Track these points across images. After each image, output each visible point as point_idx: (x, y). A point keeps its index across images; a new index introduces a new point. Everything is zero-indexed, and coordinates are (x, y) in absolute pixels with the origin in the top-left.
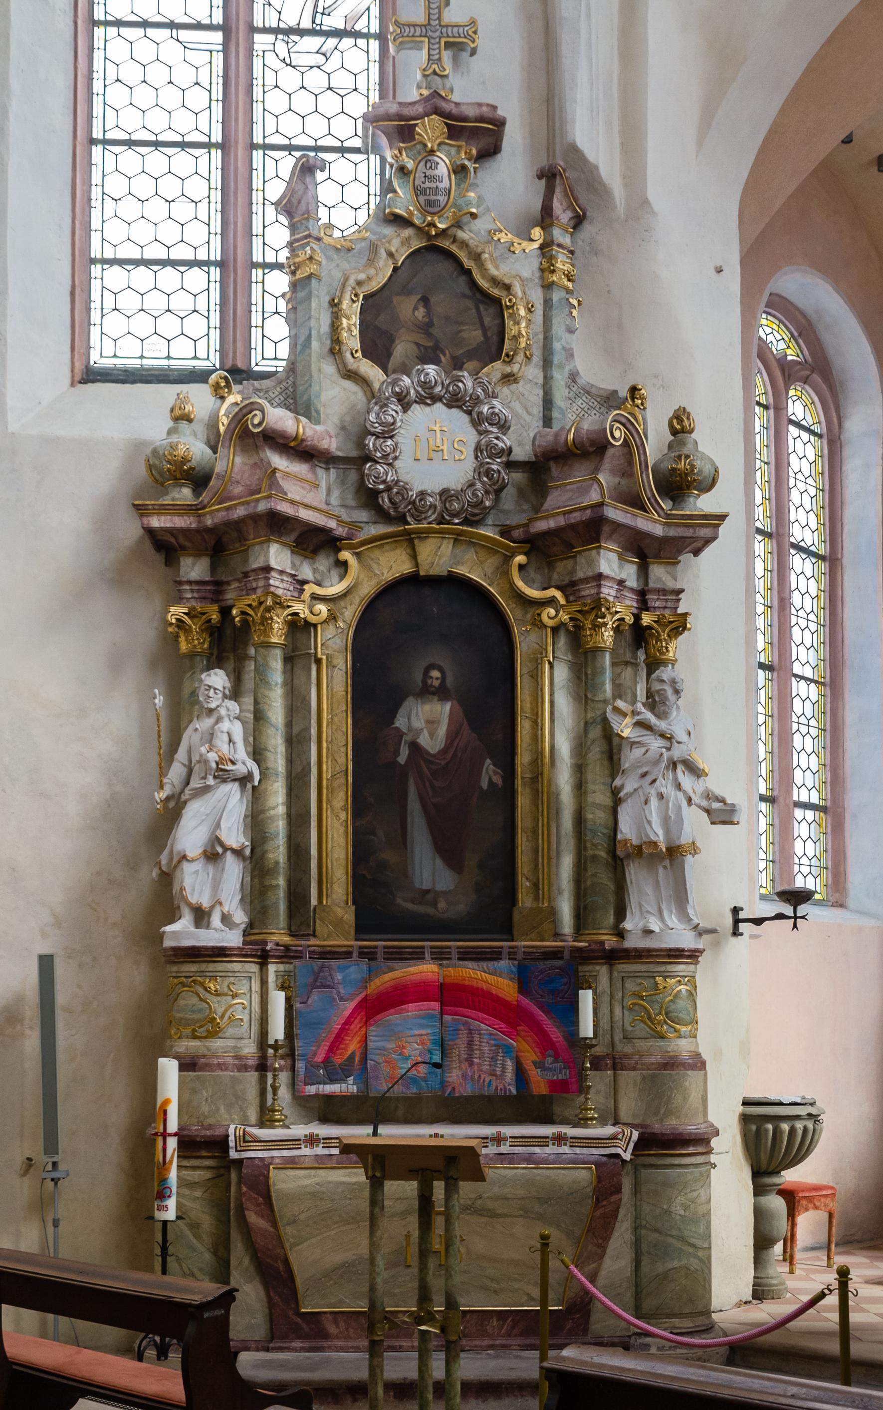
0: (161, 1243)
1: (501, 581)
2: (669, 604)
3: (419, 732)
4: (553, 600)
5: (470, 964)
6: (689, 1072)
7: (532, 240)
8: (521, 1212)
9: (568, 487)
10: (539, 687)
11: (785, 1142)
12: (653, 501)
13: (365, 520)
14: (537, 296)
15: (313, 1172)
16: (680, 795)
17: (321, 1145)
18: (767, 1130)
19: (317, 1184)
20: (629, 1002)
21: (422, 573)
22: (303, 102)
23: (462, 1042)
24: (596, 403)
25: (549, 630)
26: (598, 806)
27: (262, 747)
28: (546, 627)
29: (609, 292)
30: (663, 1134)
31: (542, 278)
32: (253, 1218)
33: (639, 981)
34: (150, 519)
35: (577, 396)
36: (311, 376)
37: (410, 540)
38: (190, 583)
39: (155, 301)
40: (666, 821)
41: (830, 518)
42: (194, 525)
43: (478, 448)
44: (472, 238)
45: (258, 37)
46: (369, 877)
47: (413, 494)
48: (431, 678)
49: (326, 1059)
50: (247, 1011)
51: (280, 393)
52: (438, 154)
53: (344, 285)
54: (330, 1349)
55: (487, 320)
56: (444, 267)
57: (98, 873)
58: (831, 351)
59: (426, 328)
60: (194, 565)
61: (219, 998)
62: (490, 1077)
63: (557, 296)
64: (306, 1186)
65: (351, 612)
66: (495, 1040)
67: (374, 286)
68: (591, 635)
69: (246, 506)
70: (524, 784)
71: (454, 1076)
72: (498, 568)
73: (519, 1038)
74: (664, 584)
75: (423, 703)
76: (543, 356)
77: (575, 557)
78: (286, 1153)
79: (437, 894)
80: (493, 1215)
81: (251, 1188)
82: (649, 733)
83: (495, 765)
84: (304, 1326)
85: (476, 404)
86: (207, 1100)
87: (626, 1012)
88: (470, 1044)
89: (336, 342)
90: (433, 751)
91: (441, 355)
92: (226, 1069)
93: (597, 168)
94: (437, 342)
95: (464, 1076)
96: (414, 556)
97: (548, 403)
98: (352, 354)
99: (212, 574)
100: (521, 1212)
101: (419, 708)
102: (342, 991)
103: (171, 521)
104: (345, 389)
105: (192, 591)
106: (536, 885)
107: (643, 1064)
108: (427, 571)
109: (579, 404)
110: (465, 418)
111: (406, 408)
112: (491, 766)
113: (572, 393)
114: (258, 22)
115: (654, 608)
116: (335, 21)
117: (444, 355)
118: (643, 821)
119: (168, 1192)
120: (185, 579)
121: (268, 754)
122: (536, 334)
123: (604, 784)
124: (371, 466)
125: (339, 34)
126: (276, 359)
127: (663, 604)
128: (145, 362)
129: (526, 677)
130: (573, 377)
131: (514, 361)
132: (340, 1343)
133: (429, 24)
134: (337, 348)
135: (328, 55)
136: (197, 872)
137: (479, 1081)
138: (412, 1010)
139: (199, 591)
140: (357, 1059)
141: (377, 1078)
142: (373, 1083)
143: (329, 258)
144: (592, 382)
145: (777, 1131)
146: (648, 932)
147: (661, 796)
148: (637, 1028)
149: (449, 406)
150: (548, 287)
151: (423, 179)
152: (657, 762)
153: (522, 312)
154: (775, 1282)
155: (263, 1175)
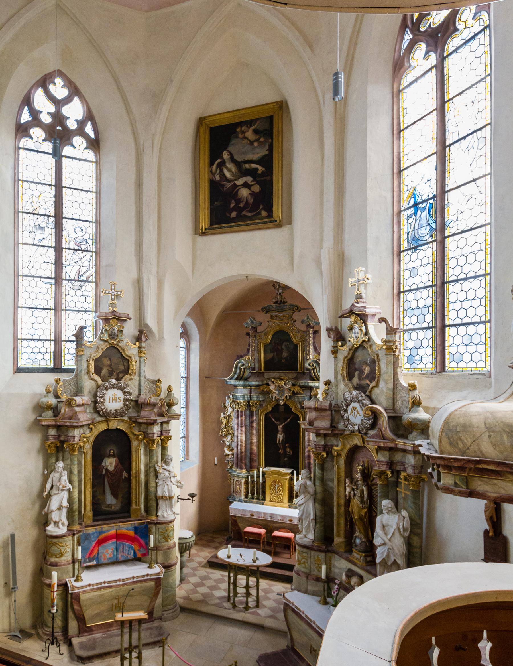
14: (137, 359)
22: (76, 299)
37: (107, 422)
40: (169, 490)
45: (64, 281)
49: (89, 557)
53: (90, 357)
55: (125, 364)
58: (188, 329)
59: (110, 366)
63: (142, 359)
65: (92, 440)
79: (112, 505)
88: (123, 548)
89: (88, 372)
96: (108, 425)
97: (140, 385)
110: (121, 392)
111: (107, 390)
118: (163, 491)
125: (85, 281)
128: (33, 366)
130: (145, 377)
132: (96, 632)
138: (110, 542)
145: (186, 545)
146: (164, 517)
150: (140, 357)
153: (134, 364)
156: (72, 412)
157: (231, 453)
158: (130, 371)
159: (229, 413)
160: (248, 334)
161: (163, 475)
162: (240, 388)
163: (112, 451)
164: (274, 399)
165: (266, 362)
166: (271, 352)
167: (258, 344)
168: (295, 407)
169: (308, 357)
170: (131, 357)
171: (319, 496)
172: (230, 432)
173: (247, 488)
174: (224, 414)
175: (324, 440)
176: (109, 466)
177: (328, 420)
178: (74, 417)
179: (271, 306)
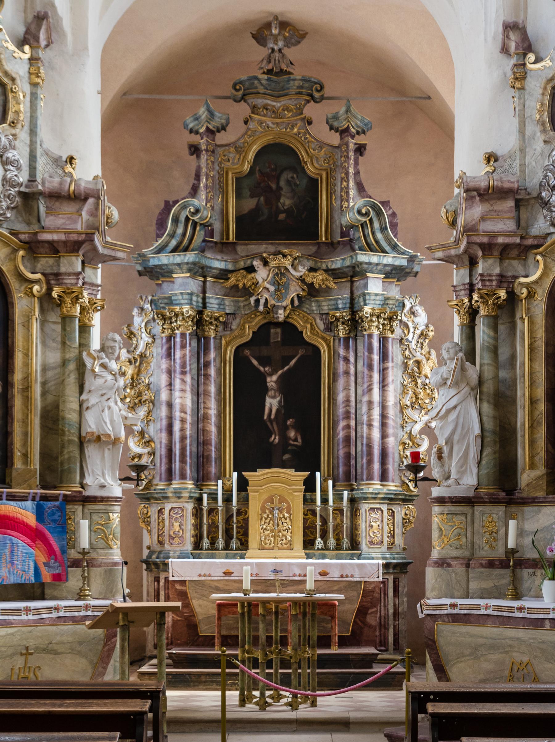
2: (94, 292)
4: (39, 281)
5: (12, 503)
7: (24, 53)
8: (70, 651)
10: (30, 333)
25: (36, 299)
28: (34, 296)
29: (58, 95)
68: (71, 307)
70: (18, 392)
72: (7, 256)
73: (36, 549)
76: (30, 126)
77: (59, 257)
82: (104, 370)
85: (5, 151)
87: (93, 533)
88: (12, 552)
93: (62, 19)
100: (70, 651)
118: (100, 421)
129: (21, 326)
144: (50, 149)
147: (109, 408)
148: (99, 542)
150: (35, 85)
152: (111, 388)
153: (21, 97)
157: (147, 450)
158: (10, 117)
159: (141, 348)
160: (195, 150)
161: (99, 381)
162: (180, 277)
164: (261, 308)
165: (239, 219)
166: (252, 196)
167: (221, 176)
168: (312, 328)
169: (345, 204)
170: (13, 80)
171: (489, 387)
172: (145, 397)
173: (198, 527)
174: (128, 352)
175: (500, 266)
177: (509, 218)
179: (256, 78)
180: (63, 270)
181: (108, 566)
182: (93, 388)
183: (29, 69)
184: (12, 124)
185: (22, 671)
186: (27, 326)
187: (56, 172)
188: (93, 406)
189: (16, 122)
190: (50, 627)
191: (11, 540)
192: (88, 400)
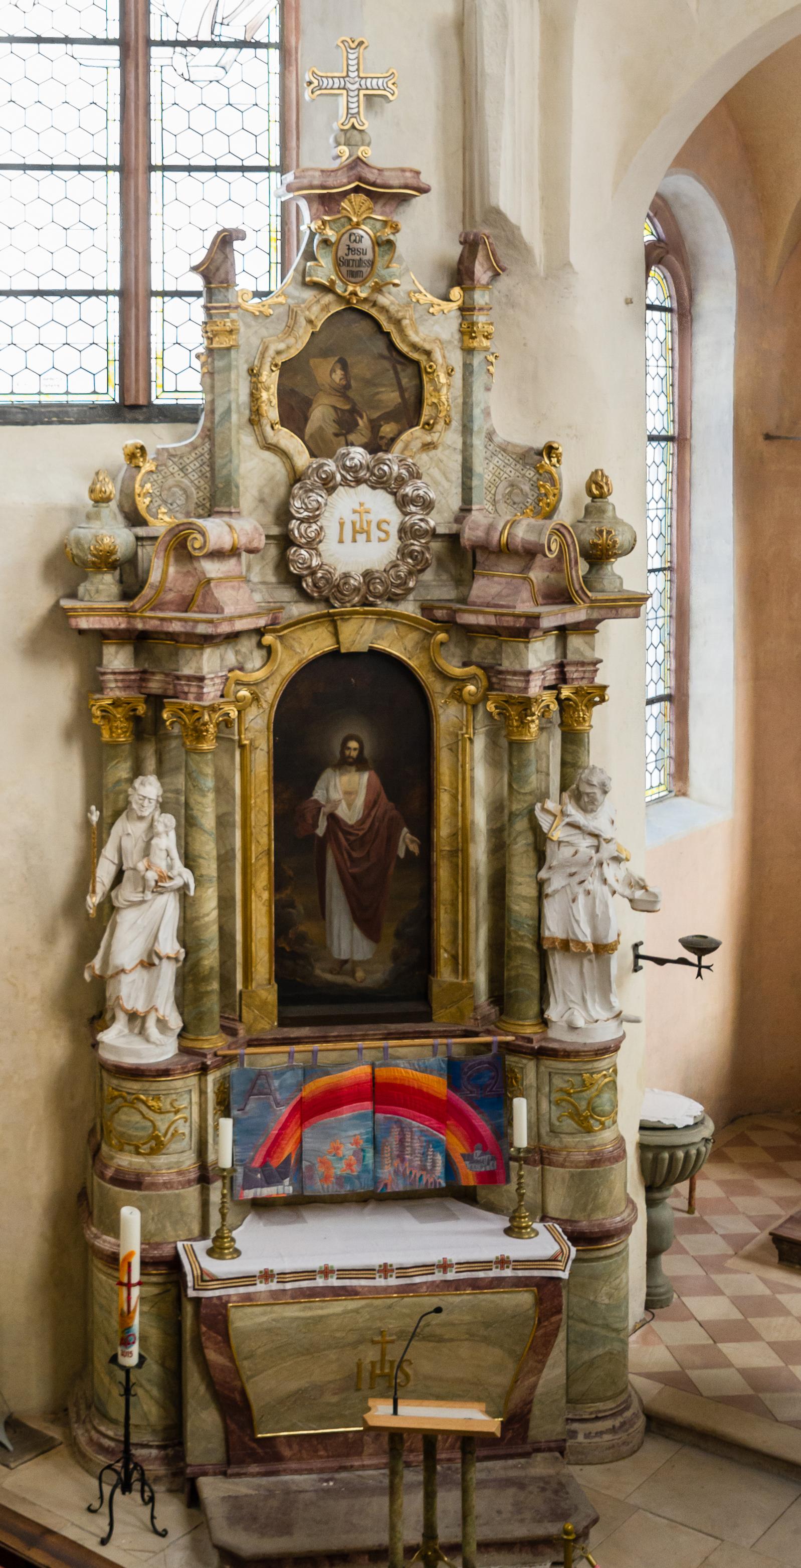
0: (124, 1383)
1: (421, 656)
3: (337, 804)
4: (474, 678)
6: (614, 1166)
8: (467, 1336)
9: (496, 579)
11: (680, 1168)
12: (580, 592)
13: (287, 600)
14: (456, 358)
15: (269, 1308)
16: (606, 889)
17: (275, 1280)
18: (663, 1160)
19: (274, 1320)
20: (555, 1096)
21: (343, 651)
23: (393, 1141)
24: (511, 460)
26: (525, 899)
27: (197, 853)
29: (525, 345)
30: (591, 1233)
31: (462, 341)
32: (212, 1355)
33: (567, 1078)
34: (78, 620)
35: (494, 454)
36: (231, 451)
37: (332, 621)
38: (114, 673)
39: (53, 335)
40: (593, 917)
41: (679, 397)
42: (123, 626)
43: (404, 531)
44: (392, 303)
45: (154, 50)
46: (288, 949)
47: (337, 576)
48: (349, 748)
49: (264, 1163)
50: (188, 1124)
51: (196, 459)
52: (363, 227)
54: (286, 1472)
55: (405, 381)
56: (361, 328)
57: (16, 948)
59: (343, 391)
60: (117, 653)
61: (162, 1116)
62: (421, 1172)
64: (263, 1323)
66: (426, 1136)
67: (293, 353)
68: (517, 727)
69: (183, 623)
71: (386, 1172)
72: (418, 643)
73: (448, 1132)
74: (582, 654)
75: (341, 774)
76: (463, 421)
78: (242, 1290)
79: (356, 964)
80: (440, 1340)
81: (210, 1327)
83: (412, 833)
84: (260, 1451)
86: (153, 1219)
87: (553, 1107)
88: (402, 1141)
89: (255, 418)
90: (351, 821)
91: (359, 419)
92: (172, 1187)
93: (519, 229)
94: (354, 405)
95: (396, 1172)
96: (336, 634)
97: (467, 470)
98: (272, 428)
99: (136, 665)
101: (338, 780)
102: (278, 1096)
103: (100, 622)
104: (263, 460)
105: (116, 681)
106: (455, 958)
107: (572, 1162)
108: (348, 649)
109: (495, 462)
110: (390, 499)
111: (331, 490)
112: (408, 835)
113: (489, 452)
114: (155, 36)
115: (573, 679)
116: (234, 32)
117: (362, 417)
118: (570, 919)
119: (131, 1339)
120: (109, 671)
121: (201, 861)
122: (455, 398)
123: (530, 876)
124: (295, 551)
126: (176, 391)
127: (581, 675)
131: (434, 430)
132: (294, 1466)
133: (348, 76)
134: (257, 419)
135: (227, 69)
136: (134, 981)
137: (410, 1176)
138: (347, 1113)
139: (122, 681)
140: (293, 1161)
141: (311, 1177)
142: (307, 1182)
143: (248, 326)
145: (672, 1158)
146: (572, 1028)
148: (564, 1123)
149: (373, 488)
150: (469, 351)
151: (347, 252)
153: (443, 379)
154: (662, 1290)
155: (221, 1314)
156: (191, 581)
161: (566, 852)
163: (353, 744)
176: (344, 804)
178: (199, 600)
180: (506, 665)
181: (577, 1167)
182: (554, 863)
183: (461, 325)
184: (427, 427)
185: (378, 1366)
186: (459, 746)
187: (524, 476)
188: (556, 892)
189: (432, 422)
190: (427, 1298)
191: (398, 1122)
192: (549, 879)
